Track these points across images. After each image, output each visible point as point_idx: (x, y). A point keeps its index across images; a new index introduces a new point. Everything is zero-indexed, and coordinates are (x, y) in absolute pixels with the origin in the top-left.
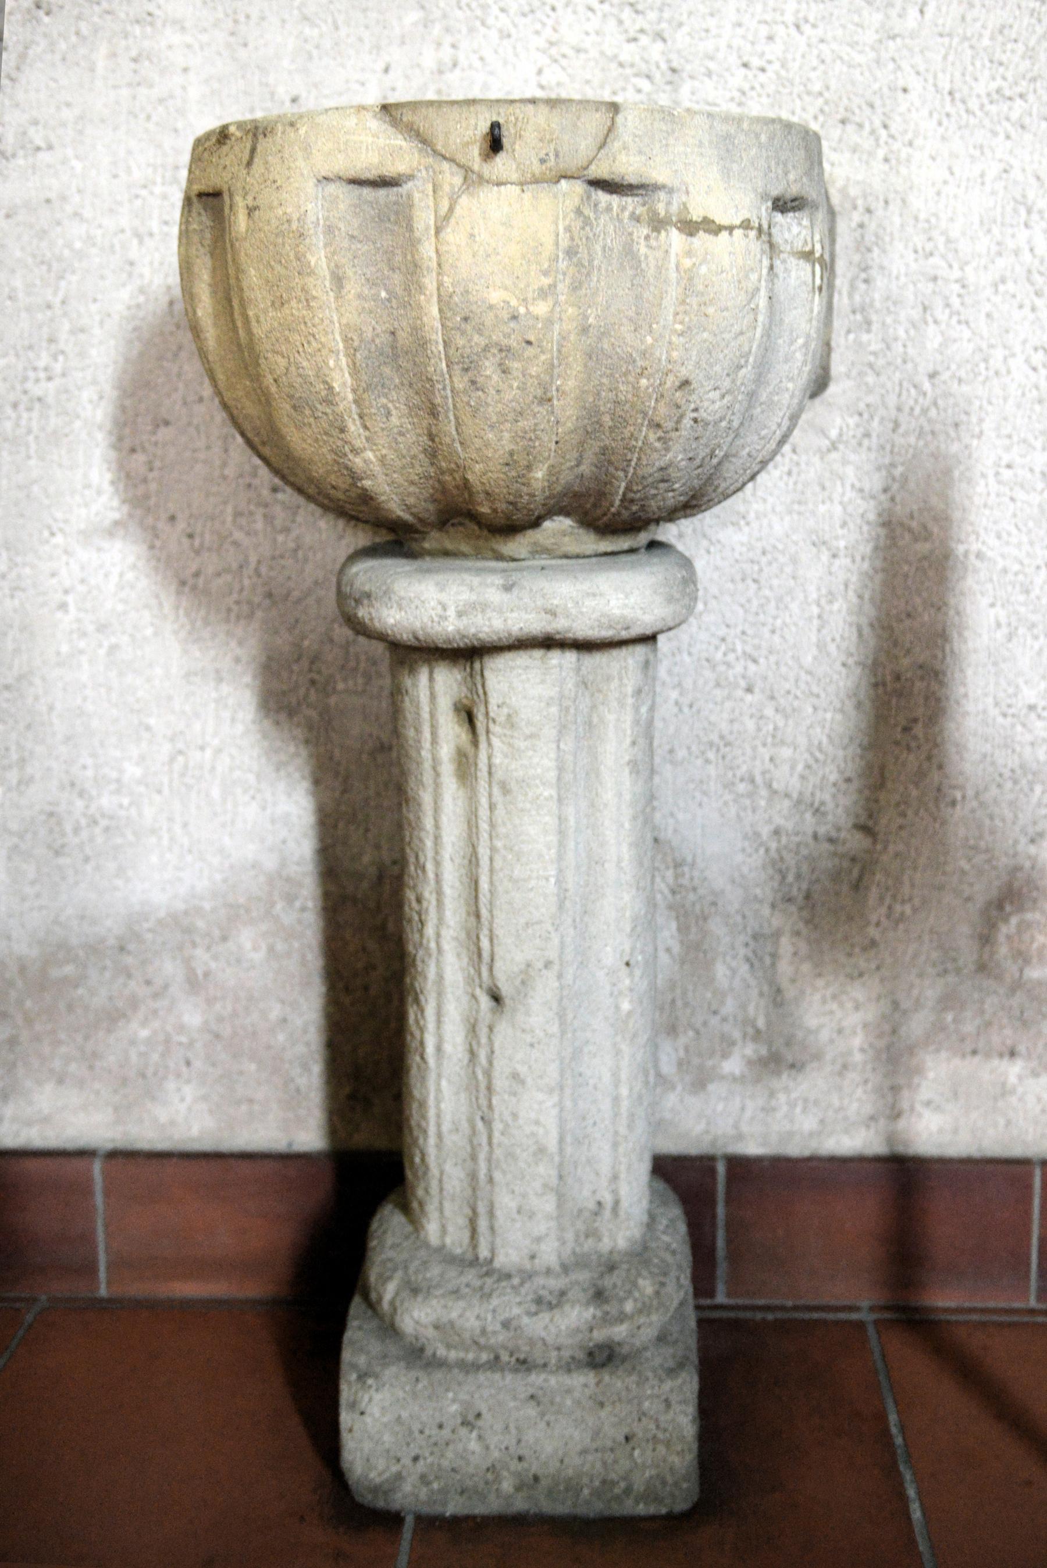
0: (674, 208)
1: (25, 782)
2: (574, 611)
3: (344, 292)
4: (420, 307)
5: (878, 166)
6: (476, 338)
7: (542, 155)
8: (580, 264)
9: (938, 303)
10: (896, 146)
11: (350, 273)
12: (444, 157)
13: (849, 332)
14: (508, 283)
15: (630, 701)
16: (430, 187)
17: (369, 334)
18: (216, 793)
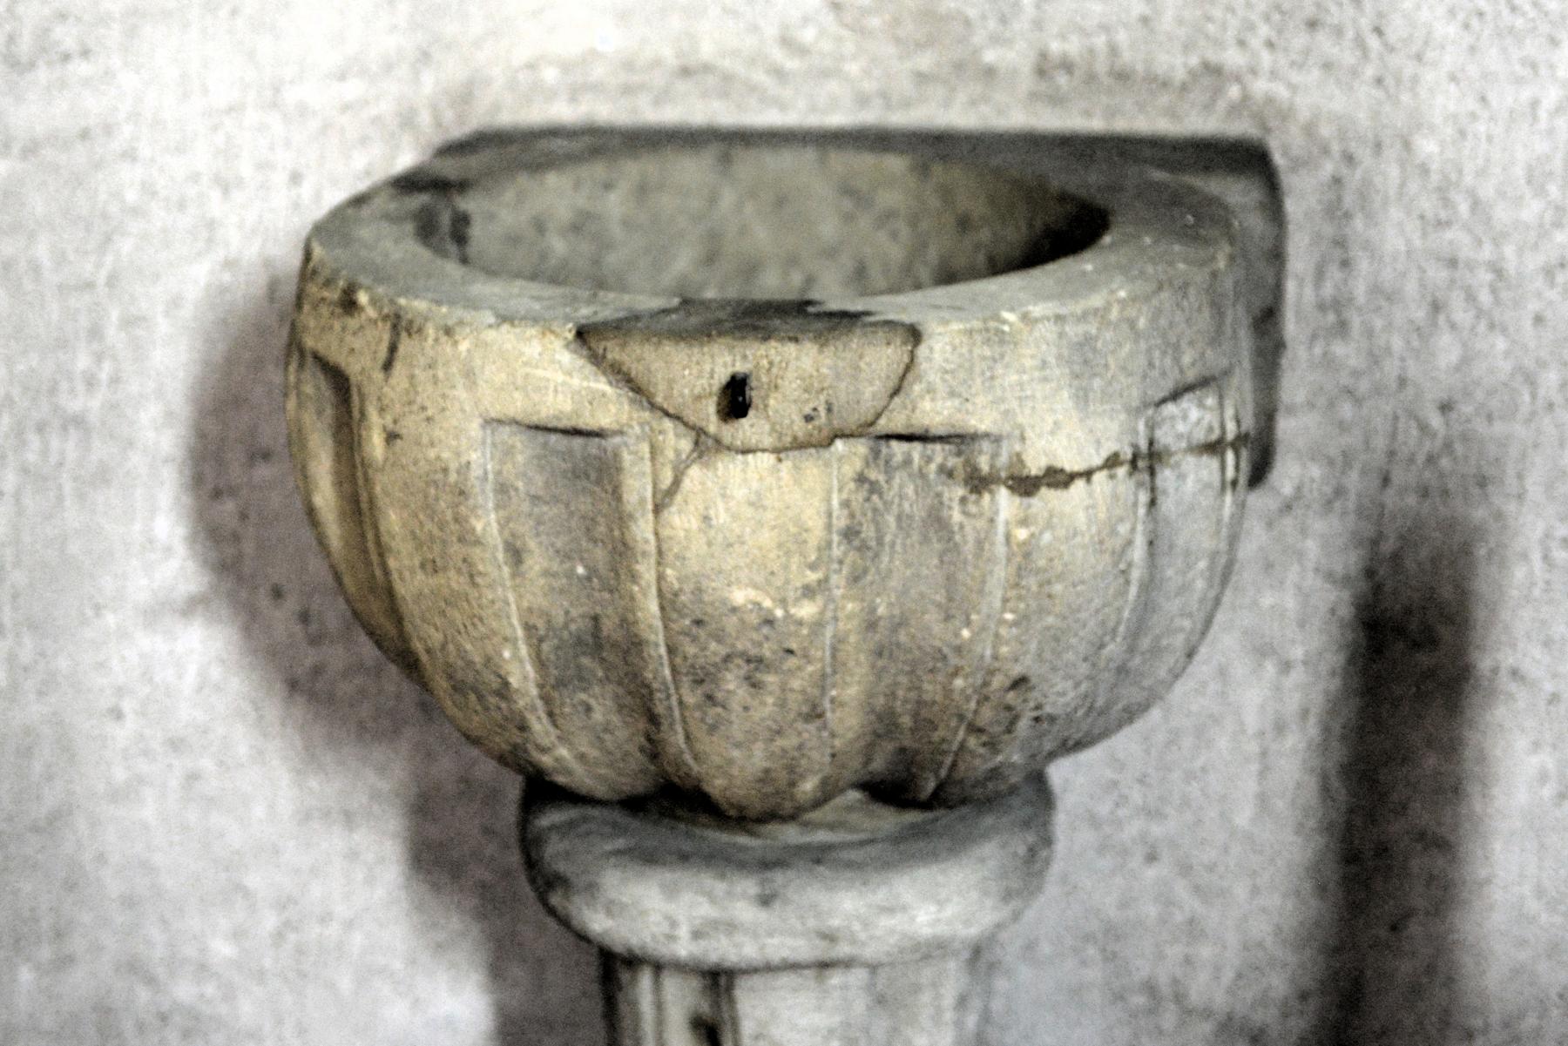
0: (1003, 460)
1: (65, 962)
2: (863, 936)
3: (524, 567)
4: (632, 598)
5: (1365, 92)
6: (713, 646)
7: (807, 410)
8: (863, 548)
9: (1457, 302)
10: (1395, 61)
11: (532, 544)
12: (667, 414)
13: (1314, 337)
14: (759, 579)
15: (949, 1016)
16: (645, 448)
17: (560, 619)
18: (345, 983)
